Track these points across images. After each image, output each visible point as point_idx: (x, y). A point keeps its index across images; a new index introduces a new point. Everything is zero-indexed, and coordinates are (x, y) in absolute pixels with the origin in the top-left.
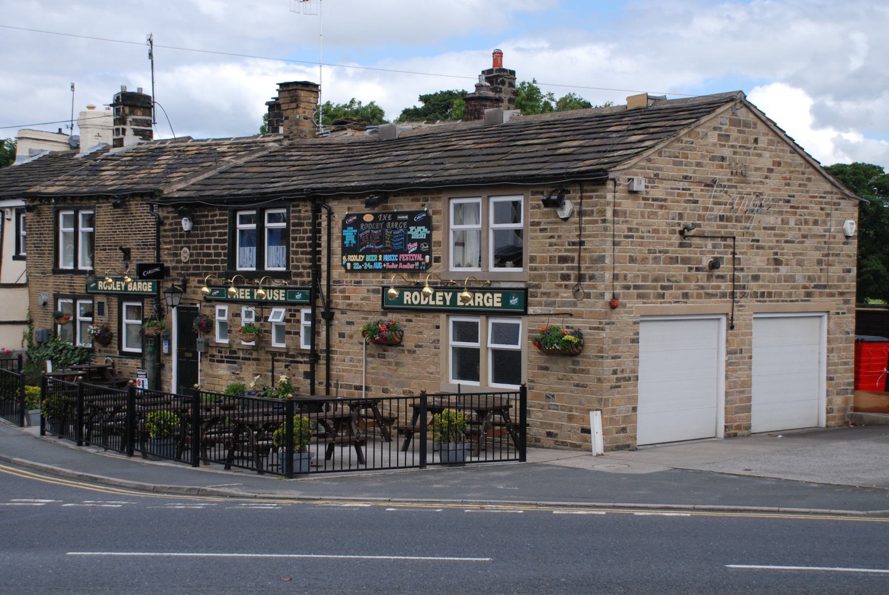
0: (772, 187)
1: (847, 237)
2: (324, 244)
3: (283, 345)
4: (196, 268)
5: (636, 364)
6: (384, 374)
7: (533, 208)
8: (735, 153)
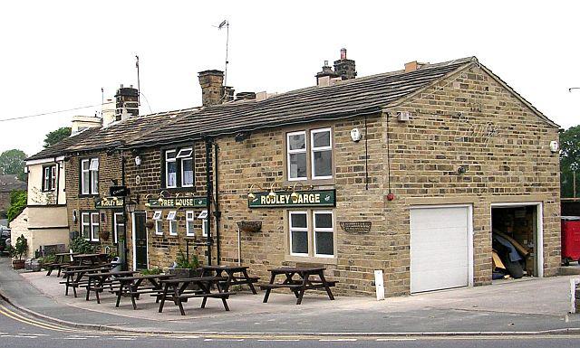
0: (499, 119)
1: (553, 152)
3: (193, 235)
5: (408, 238)
8: (473, 96)
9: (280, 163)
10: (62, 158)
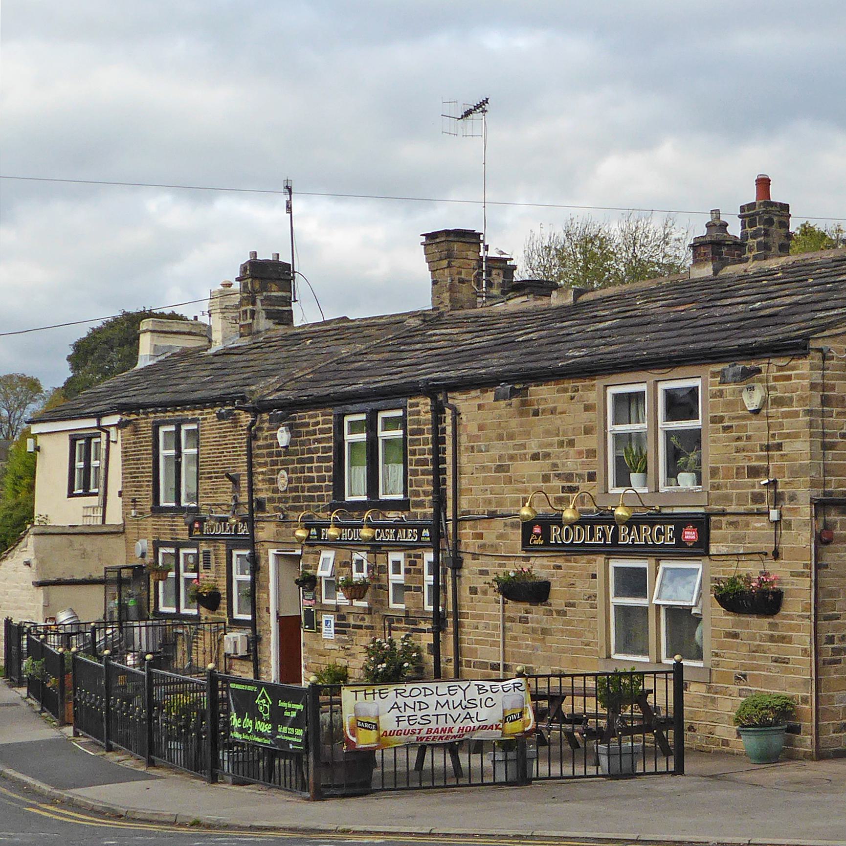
2: (449, 459)
3: (402, 606)
4: (296, 499)
6: (527, 646)
7: (714, 396)
9: (591, 453)
10: (115, 419)
